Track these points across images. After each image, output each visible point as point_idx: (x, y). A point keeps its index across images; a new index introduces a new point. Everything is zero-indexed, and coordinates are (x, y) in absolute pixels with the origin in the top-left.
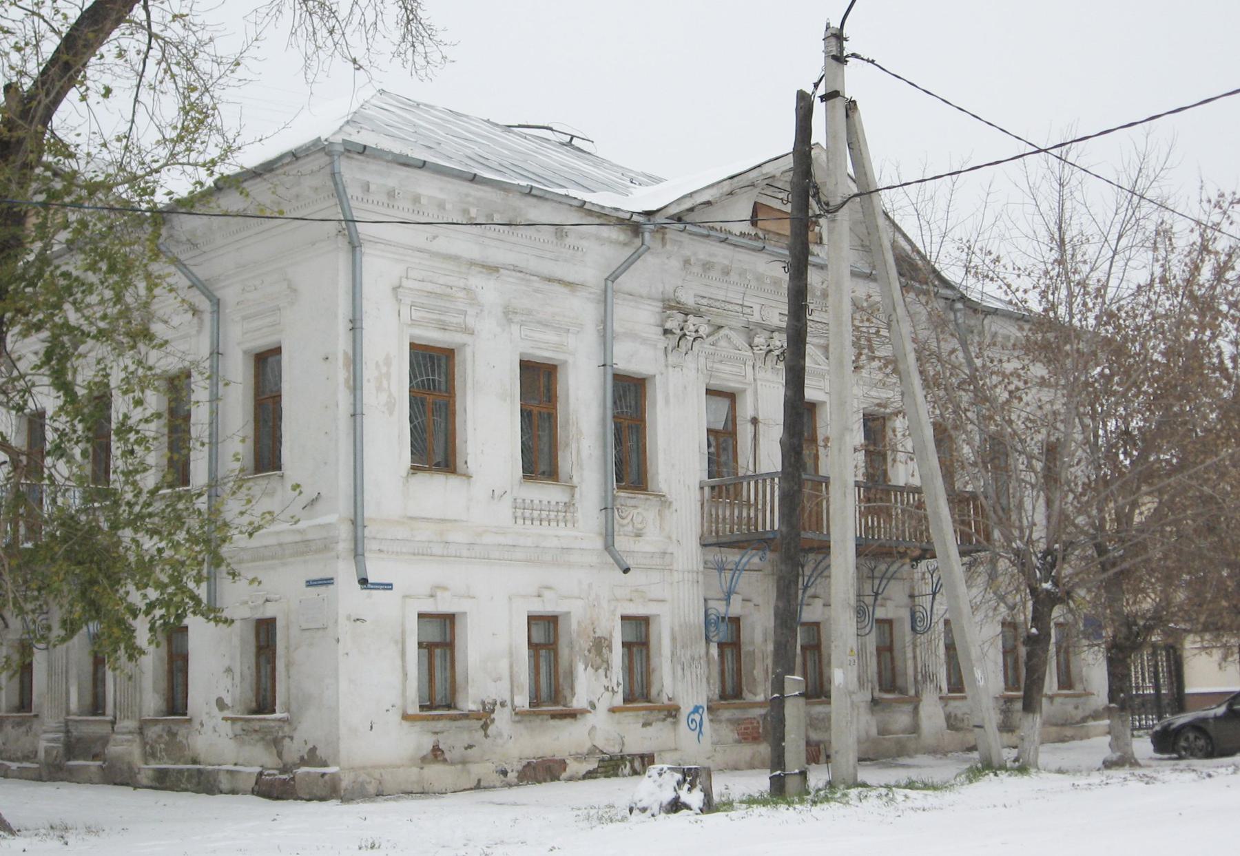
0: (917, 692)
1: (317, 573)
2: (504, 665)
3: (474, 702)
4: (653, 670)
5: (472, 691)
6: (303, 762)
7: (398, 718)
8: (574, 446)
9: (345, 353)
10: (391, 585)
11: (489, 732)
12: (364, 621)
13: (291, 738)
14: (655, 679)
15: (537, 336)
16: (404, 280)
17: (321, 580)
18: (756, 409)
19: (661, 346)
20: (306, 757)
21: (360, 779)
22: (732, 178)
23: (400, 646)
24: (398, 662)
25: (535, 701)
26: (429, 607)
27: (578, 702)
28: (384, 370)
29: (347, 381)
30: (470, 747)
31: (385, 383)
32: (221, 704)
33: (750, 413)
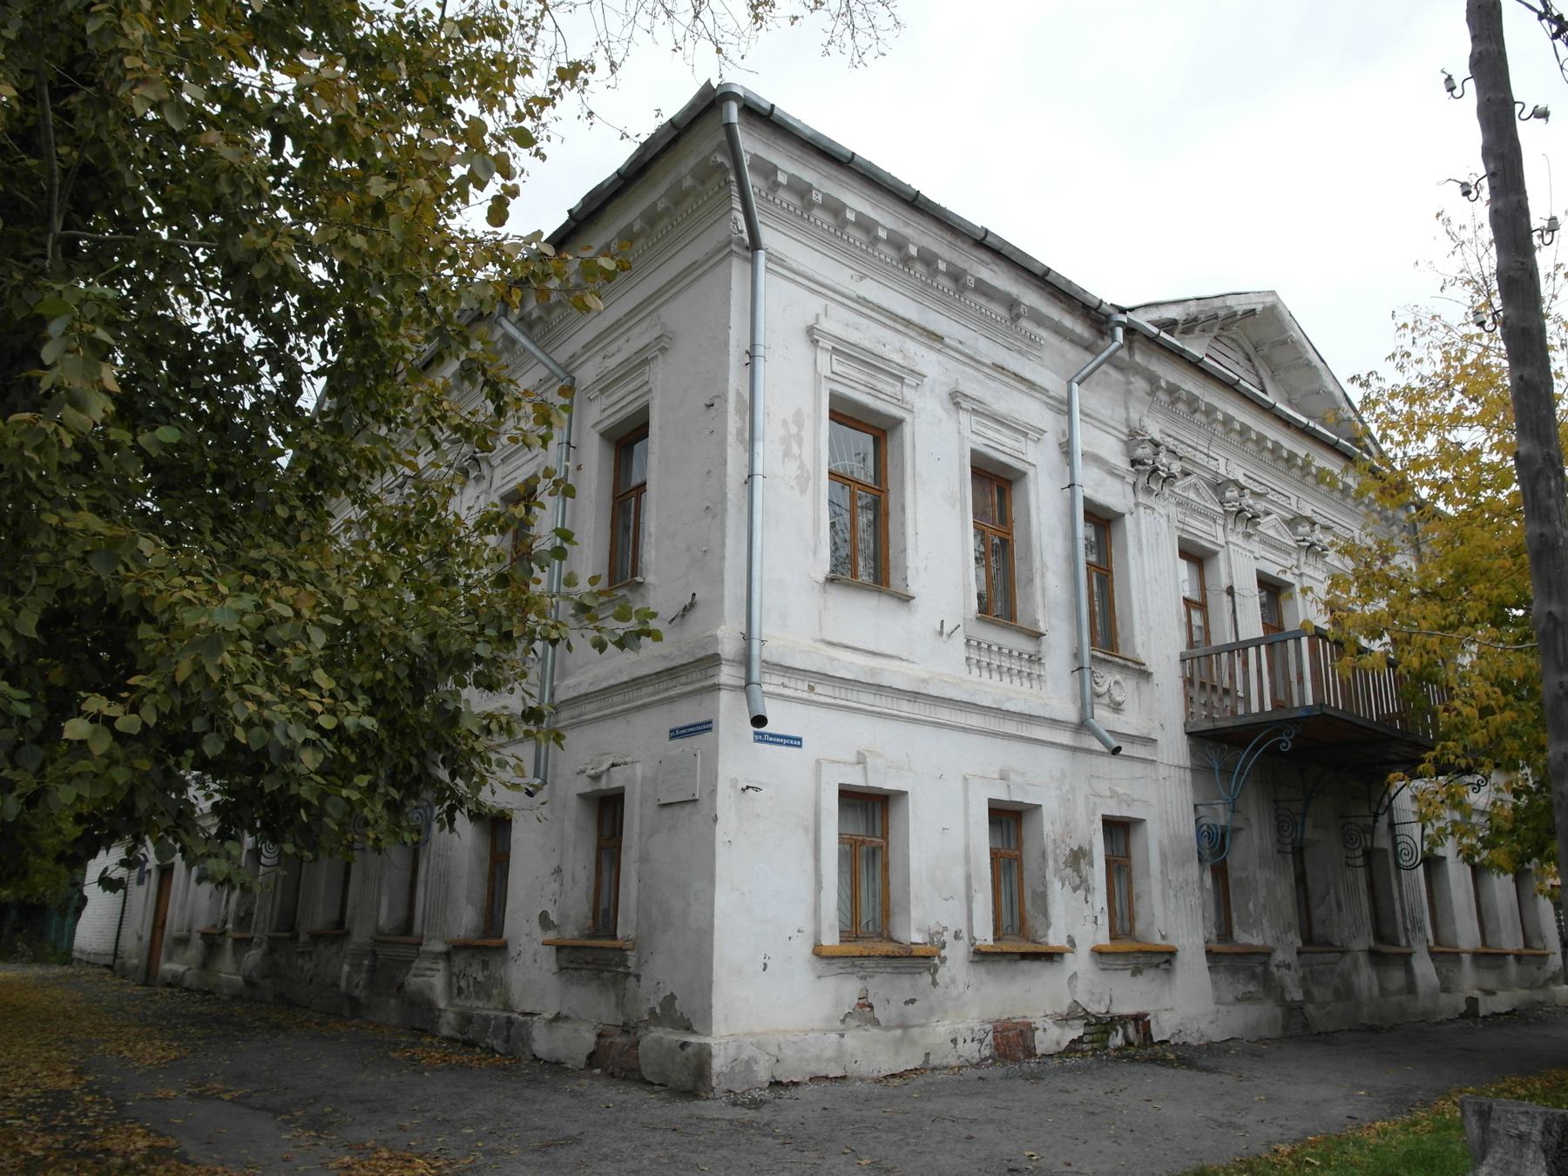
0: (1408, 941)
1: (687, 714)
2: (958, 874)
3: (919, 930)
4: (1138, 897)
5: (916, 913)
6: (656, 1019)
7: (807, 950)
8: (1038, 581)
9: (739, 395)
10: (800, 740)
11: (938, 977)
12: (757, 789)
13: (638, 977)
14: (1141, 908)
15: (990, 434)
16: (822, 317)
17: (678, 275)
18: (1231, 577)
19: (1130, 479)
20: (658, 1011)
21: (745, 1056)
22: (1198, 299)
23: (811, 835)
24: (809, 863)
25: (850, 933)
26: (856, 779)
27: (1055, 938)
28: (794, 429)
29: (740, 432)
30: (912, 1001)
31: (795, 449)
32: (544, 920)
33: (1225, 583)
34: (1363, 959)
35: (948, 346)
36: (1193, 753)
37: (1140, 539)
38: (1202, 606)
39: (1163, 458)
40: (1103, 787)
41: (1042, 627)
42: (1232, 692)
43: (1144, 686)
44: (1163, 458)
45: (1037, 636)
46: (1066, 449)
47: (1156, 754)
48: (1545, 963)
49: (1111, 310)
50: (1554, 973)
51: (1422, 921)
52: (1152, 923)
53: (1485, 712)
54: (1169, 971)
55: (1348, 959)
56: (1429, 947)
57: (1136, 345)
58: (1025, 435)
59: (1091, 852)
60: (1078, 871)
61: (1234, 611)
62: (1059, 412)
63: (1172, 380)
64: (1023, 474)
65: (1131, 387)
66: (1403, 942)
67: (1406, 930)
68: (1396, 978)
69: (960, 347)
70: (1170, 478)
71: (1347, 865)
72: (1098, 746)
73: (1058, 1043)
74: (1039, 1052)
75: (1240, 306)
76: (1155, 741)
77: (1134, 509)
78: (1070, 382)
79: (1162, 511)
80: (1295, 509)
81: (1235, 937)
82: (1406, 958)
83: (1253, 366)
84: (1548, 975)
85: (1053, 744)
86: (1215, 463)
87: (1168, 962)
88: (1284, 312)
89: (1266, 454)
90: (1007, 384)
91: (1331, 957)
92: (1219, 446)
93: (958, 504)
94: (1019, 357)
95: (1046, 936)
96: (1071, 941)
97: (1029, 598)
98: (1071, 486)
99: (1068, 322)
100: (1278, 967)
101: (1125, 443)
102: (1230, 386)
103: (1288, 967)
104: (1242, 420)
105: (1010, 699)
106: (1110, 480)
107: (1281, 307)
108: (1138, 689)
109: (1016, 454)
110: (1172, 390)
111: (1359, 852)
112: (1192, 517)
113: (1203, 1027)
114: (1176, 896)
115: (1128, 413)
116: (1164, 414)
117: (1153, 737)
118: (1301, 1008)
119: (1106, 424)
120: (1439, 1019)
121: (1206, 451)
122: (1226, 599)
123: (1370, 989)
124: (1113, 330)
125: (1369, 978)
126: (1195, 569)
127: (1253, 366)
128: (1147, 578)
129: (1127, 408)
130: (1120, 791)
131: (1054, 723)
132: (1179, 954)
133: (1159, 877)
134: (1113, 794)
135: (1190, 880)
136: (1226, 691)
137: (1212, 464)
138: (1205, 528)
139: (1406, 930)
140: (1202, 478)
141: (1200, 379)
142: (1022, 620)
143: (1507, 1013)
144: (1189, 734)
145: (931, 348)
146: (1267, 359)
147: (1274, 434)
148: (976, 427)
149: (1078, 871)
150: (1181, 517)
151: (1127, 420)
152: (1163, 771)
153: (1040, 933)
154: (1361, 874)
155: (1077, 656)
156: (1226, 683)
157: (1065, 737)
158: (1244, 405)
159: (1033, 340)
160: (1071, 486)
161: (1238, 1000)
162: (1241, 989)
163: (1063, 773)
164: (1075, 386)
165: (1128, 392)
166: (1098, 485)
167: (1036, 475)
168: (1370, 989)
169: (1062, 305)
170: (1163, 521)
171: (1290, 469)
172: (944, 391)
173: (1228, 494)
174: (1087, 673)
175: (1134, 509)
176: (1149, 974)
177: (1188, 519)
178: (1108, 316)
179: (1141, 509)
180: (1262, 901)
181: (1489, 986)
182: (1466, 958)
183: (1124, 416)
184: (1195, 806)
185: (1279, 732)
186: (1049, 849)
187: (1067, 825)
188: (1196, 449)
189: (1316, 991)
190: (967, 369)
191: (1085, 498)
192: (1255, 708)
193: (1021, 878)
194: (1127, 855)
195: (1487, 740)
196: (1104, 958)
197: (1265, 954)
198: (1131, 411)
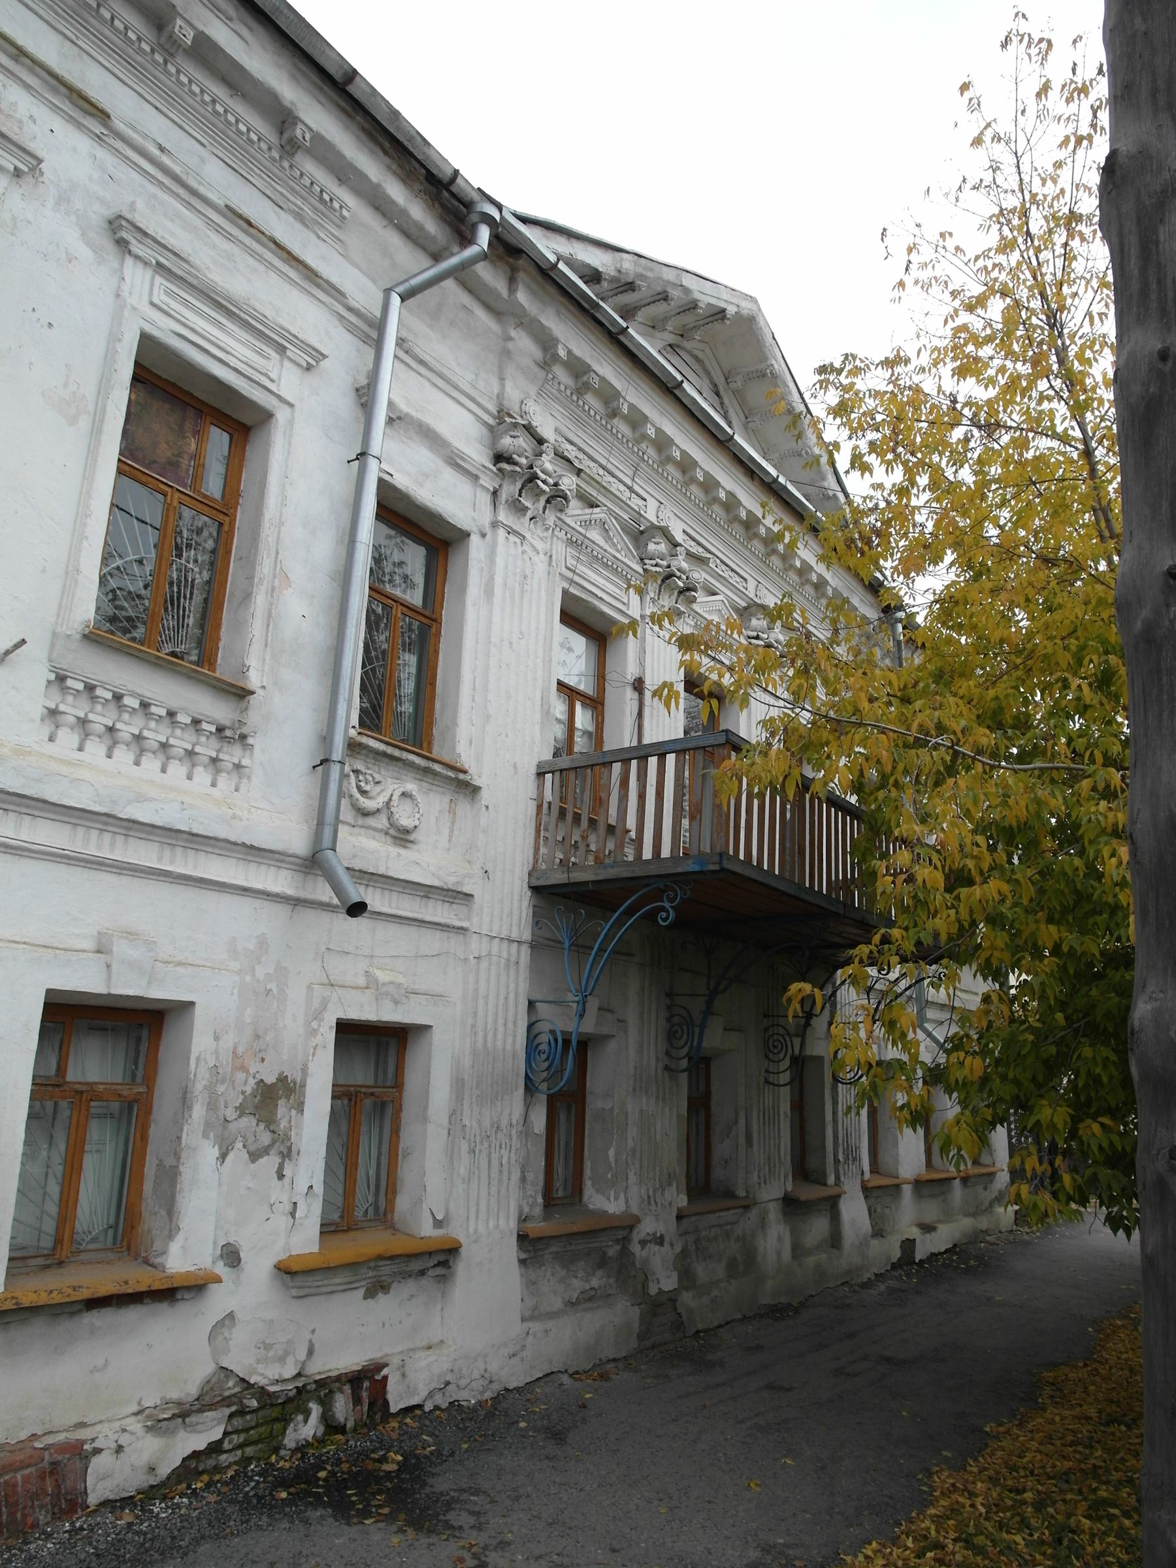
0: (838, 1178)
4: (407, 1154)
14: (407, 1173)
18: (642, 664)
33: (632, 672)
34: (774, 1212)
35: (119, 135)
36: (538, 918)
37: (492, 578)
38: (596, 703)
39: (547, 462)
40: (351, 971)
41: (254, 680)
42: (618, 831)
43: (463, 807)
44: (547, 462)
45: (241, 694)
46: (365, 396)
47: (469, 919)
48: (991, 1182)
49: (476, 196)
50: (1000, 1191)
51: (858, 1148)
52: (420, 1201)
53: (957, 879)
54: (443, 1279)
55: (754, 1213)
56: (863, 1181)
57: (521, 275)
58: (282, 350)
59: (303, 1086)
60: (269, 1121)
61: (640, 715)
62: (365, 339)
63: (577, 352)
64: (267, 416)
65: (510, 345)
66: (831, 1180)
67: (837, 1161)
68: (819, 1227)
69: (165, 160)
70: (557, 498)
71: (767, 1082)
72: (325, 893)
73: (152, 1469)
74: (93, 1500)
75: (706, 297)
76: (469, 896)
77: (488, 530)
78: (388, 292)
79: (540, 545)
80: (752, 595)
81: (585, 1198)
82: (832, 1203)
83: (722, 404)
84: (995, 1194)
85: (245, 891)
86: (641, 502)
87: (444, 1264)
88: (766, 330)
89: (716, 508)
90: (260, 259)
91: (728, 1216)
92: (650, 481)
93: (84, 423)
94: (298, 226)
95: (164, 1253)
96: (231, 1256)
97: (241, 626)
98: (362, 455)
99: (396, 191)
100: (643, 1243)
101: (490, 428)
102: (669, 390)
103: (660, 1240)
104: (684, 447)
105: (141, 799)
106: (449, 474)
107: (762, 323)
108: (452, 811)
109: (256, 376)
110: (578, 369)
111: (786, 1063)
112: (591, 567)
113: (493, 1367)
114: (472, 1151)
115: (503, 386)
116: (565, 407)
117: (466, 889)
118: (673, 1301)
119: (456, 388)
120: (867, 1275)
121: (628, 481)
122: (630, 695)
123: (779, 1253)
124: (474, 228)
125: (780, 1239)
126: (594, 649)
127: (722, 404)
128: (494, 639)
129: (502, 379)
130: (382, 976)
131: (252, 852)
132: (463, 1251)
133: (445, 1122)
134: (371, 983)
135: (504, 1122)
136: (611, 829)
137: (635, 502)
138: (611, 588)
139: (837, 1161)
140: (617, 518)
141: (624, 365)
142: (224, 671)
143: (946, 1251)
144: (536, 890)
145: (79, 126)
146: (738, 394)
147: (730, 481)
148: (160, 297)
149: (269, 1121)
150: (571, 562)
151: (500, 397)
152: (476, 946)
153: (157, 1245)
154: (785, 1095)
155: (326, 739)
156: (612, 821)
157: (280, 881)
158: (688, 425)
159: (325, 203)
160: (362, 455)
161: (571, 1304)
162: (578, 1285)
163: (262, 943)
164: (395, 300)
165: (505, 354)
166: (427, 476)
167: (291, 422)
168: (779, 1253)
169: (386, 159)
170: (541, 562)
171: (750, 539)
172: (98, 213)
173: (651, 547)
174: (335, 771)
175: (488, 530)
176: (403, 1290)
177: (581, 568)
178: (468, 205)
179: (501, 533)
180: (630, 1144)
181: (928, 1219)
182: (907, 1190)
183: (496, 390)
184: (531, 1004)
185: (657, 895)
186: (199, 1086)
187: (257, 1037)
188: (614, 476)
189: (701, 1271)
190: (166, 197)
191: (381, 481)
192: (647, 854)
193: (144, 1138)
194: (398, 1085)
195: (954, 929)
196: (299, 1281)
197: (625, 1226)
198: (509, 385)
